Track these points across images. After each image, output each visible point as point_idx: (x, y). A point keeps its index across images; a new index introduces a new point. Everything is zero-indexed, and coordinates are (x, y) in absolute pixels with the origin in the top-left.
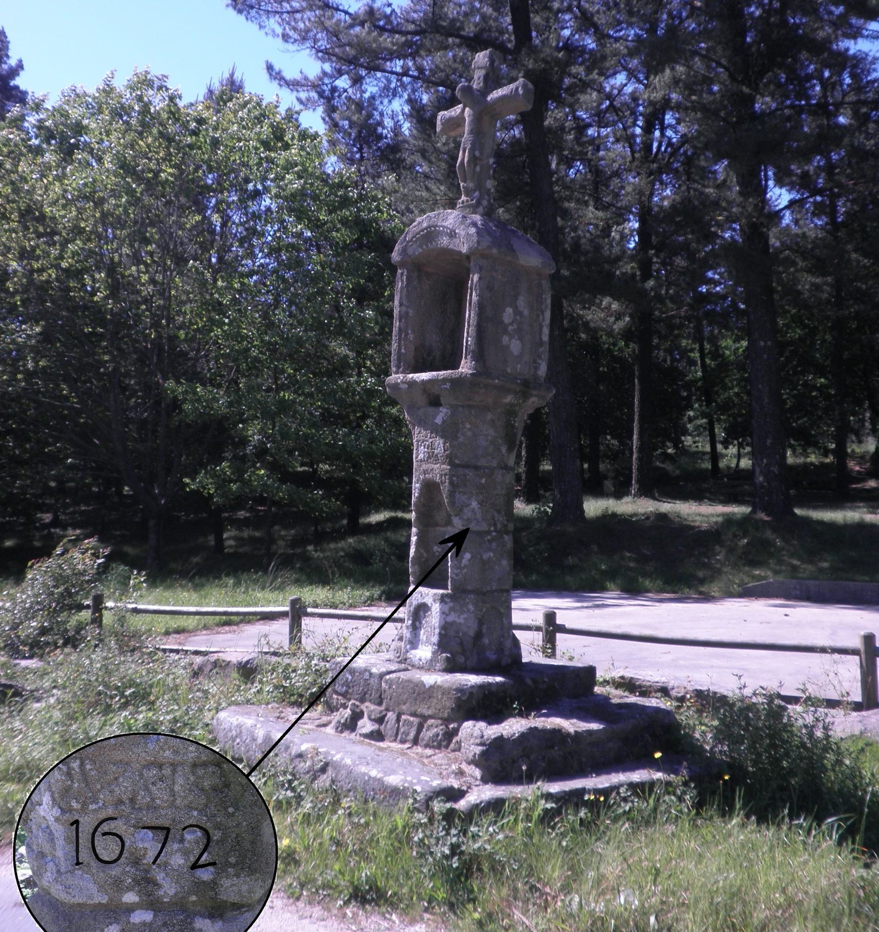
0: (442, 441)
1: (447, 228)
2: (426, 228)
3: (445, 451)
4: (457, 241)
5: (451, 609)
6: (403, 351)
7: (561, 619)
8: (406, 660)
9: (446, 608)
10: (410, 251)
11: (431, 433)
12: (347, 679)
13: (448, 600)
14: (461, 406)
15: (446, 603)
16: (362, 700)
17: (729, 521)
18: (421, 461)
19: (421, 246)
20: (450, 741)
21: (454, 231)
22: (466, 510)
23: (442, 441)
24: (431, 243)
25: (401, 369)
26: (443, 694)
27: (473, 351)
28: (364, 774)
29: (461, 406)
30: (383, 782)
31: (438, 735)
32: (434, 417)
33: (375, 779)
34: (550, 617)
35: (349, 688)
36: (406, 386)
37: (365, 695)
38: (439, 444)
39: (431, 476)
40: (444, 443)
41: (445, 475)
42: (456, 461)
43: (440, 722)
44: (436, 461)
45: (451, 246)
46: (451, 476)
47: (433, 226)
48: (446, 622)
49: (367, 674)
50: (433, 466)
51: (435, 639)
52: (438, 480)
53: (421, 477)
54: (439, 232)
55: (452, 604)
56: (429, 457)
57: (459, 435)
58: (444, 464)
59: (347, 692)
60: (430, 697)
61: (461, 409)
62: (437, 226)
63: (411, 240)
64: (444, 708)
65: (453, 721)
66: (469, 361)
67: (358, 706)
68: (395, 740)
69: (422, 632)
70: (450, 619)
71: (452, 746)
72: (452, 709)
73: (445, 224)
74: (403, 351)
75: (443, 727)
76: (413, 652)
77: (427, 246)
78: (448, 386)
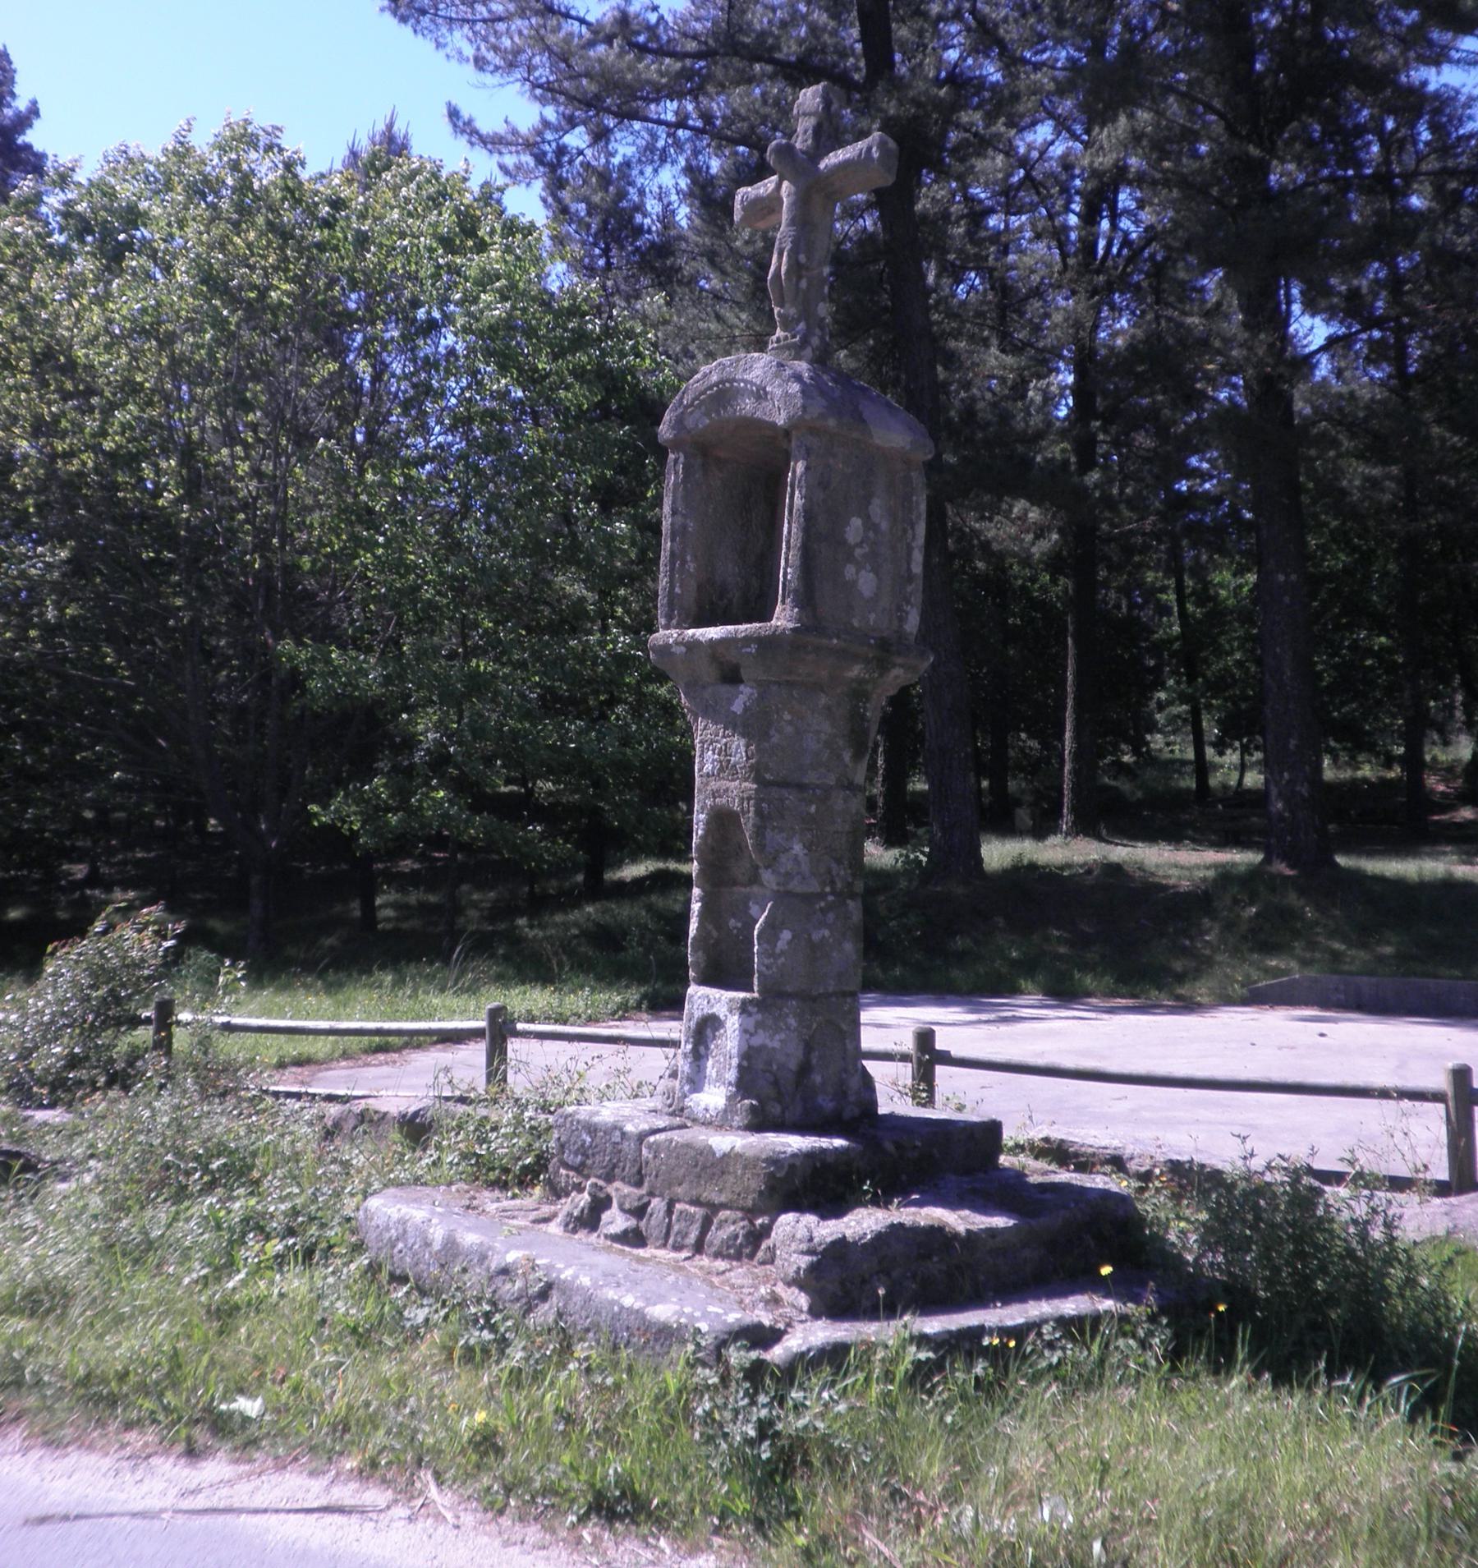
0: (742, 742)
2: (717, 384)
3: (748, 758)
4: (768, 405)
5: (759, 1025)
6: (677, 590)
9: (751, 1023)
10: (689, 423)
11: (725, 728)
15: (750, 1015)
16: (609, 1178)
17: (1226, 877)
18: (708, 775)
19: (707, 414)
20: (757, 1247)
21: (764, 389)
23: (742, 742)
24: (725, 409)
25: (674, 622)
26: (745, 1167)
27: (796, 591)
28: (613, 1303)
29: (776, 683)
30: (644, 1316)
31: (736, 1237)
32: (730, 702)
33: (630, 1311)
34: (925, 1038)
36: (683, 649)
39: (724, 801)
40: (747, 746)
41: (749, 799)
42: (768, 776)
43: (739, 1214)
44: (734, 775)
45: (758, 414)
49: (618, 1133)
51: (731, 1075)
52: (736, 807)
53: (709, 802)
54: (738, 390)
55: (759, 1017)
56: (721, 770)
57: (772, 732)
58: (746, 780)
59: (583, 1164)
60: (723, 1173)
61: (774, 688)
62: (734, 380)
63: (692, 405)
64: (747, 1190)
65: (762, 1213)
66: (788, 607)
68: (664, 1245)
69: (710, 1063)
70: (756, 1041)
71: (760, 1254)
72: (761, 1193)
73: (748, 377)
74: (677, 590)
75: (745, 1223)
77: (718, 413)
78: (753, 649)
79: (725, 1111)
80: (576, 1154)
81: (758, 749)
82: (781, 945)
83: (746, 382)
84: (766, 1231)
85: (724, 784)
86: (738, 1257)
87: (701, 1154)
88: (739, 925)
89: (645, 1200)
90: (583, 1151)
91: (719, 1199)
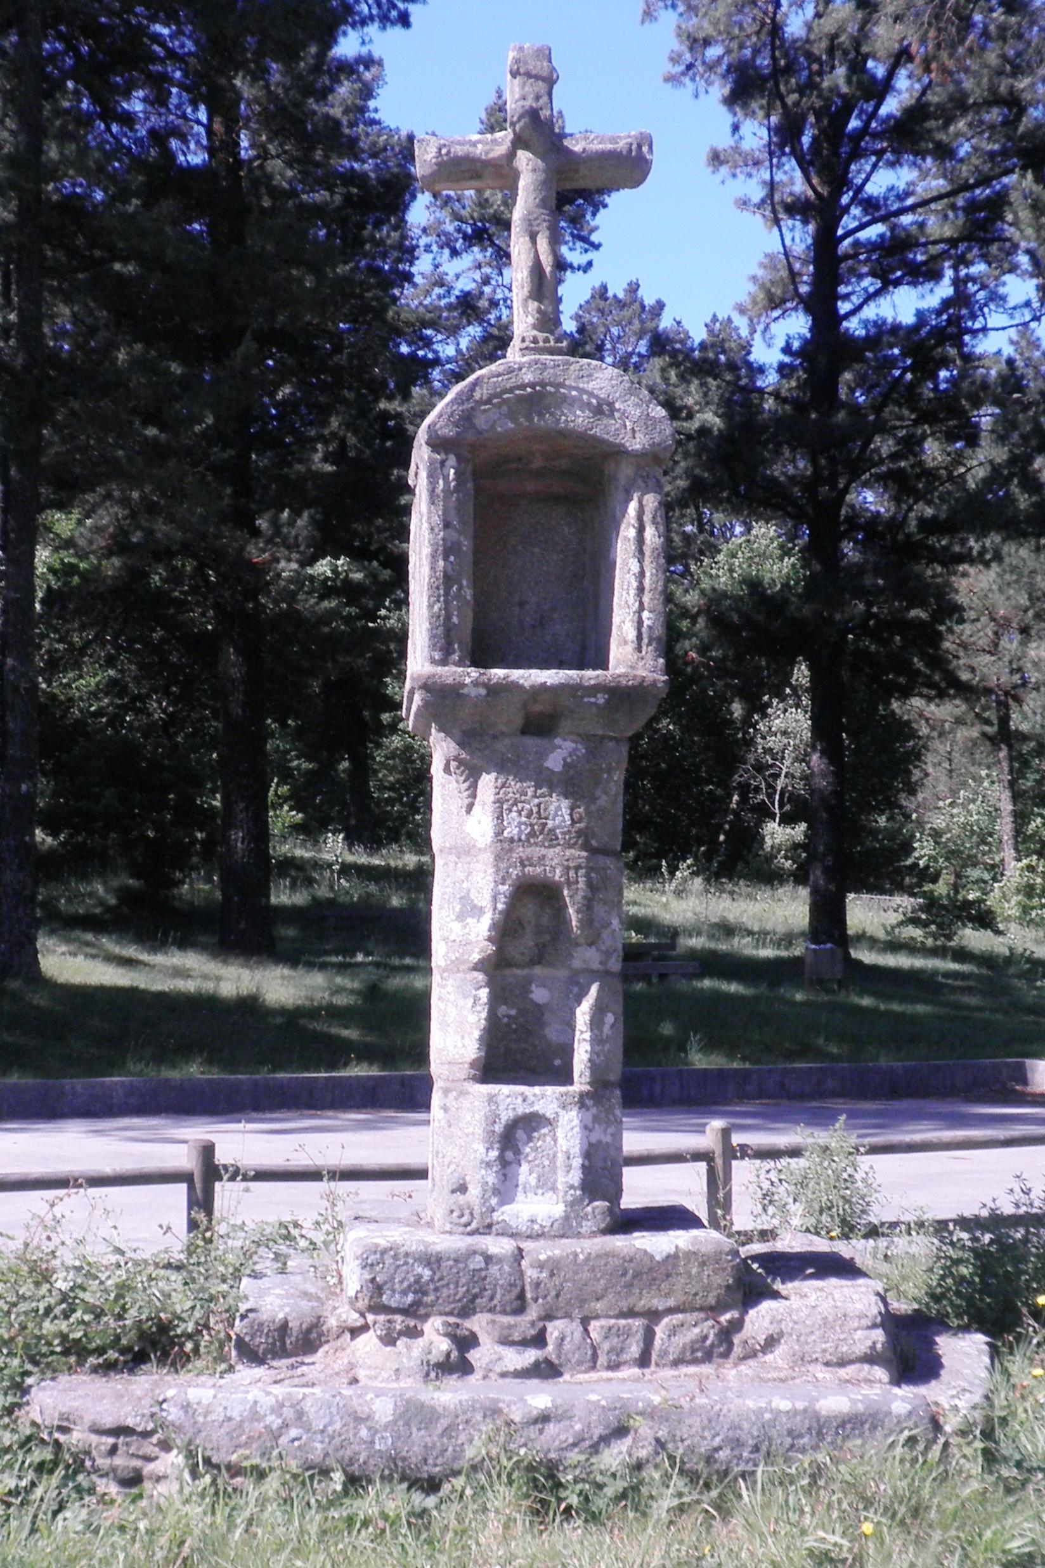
0: (565, 804)
1: (591, 394)
2: (532, 385)
3: (573, 822)
4: (613, 424)
5: (596, 1119)
6: (455, 620)
7: (222, 1157)
8: (490, 1226)
9: (589, 1116)
10: (481, 422)
11: (538, 786)
12: (420, 1276)
13: (589, 1102)
14: (612, 738)
15: (588, 1109)
18: (512, 840)
19: (511, 415)
20: (731, 1345)
21: (611, 405)
22: (605, 934)
24: (541, 415)
25: (456, 657)
26: (703, 1264)
27: (659, 639)
28: (759, 1412)
29: (612, 738)
31: (705, 1338)
32: (542, 755)
34: (208, 1151)
35: (425, 1293)
36: (483, 691)
37: (473, 1300)
38: (559, 808)
39: (539, 870)
40: (572, 809)
41: (577, 868)
42: (594, 843)
43: (702, 1315)
44: (551, 838)
45: (597, 431)
46: (590, 869)
47: (551, 384)
48: (590, 1145)
49: (479, 1258)
50: (543, 851)
52: (558, 875)
53: (514, 872)
54: (565, 398)
55: (594, 1110)
56: (532, 834)
57: (598, 793)
58: (571, 846)
59: (417, 1304)
60: (668, 1276)
61: (611, 745)
62: (562, 385)
63: (489, 401)
64: (708, 1288)
66: (649, 656)
67: (458, 1325)
68: (593, 1367)
69: (525, 1168)
70: (594, 1138)
72: (728, 1287)
73: (590, 386)
74: (455, 620)
75: (711, 1323)
76: (506, 1208)
77: (529, 418)
78: (601, 699)
79: (567, 1218)
80: (404, 1293)
81: (588, 812)
82: (606, 1029)
83: (582, 391)
84: (737, 1325)
85: (537, 851)
86: (708, 1357)
87: (631, 1261)
88: (513, 1012)
89: (541, 1324)
90: (418, 1287)
91: (660, 1304)
